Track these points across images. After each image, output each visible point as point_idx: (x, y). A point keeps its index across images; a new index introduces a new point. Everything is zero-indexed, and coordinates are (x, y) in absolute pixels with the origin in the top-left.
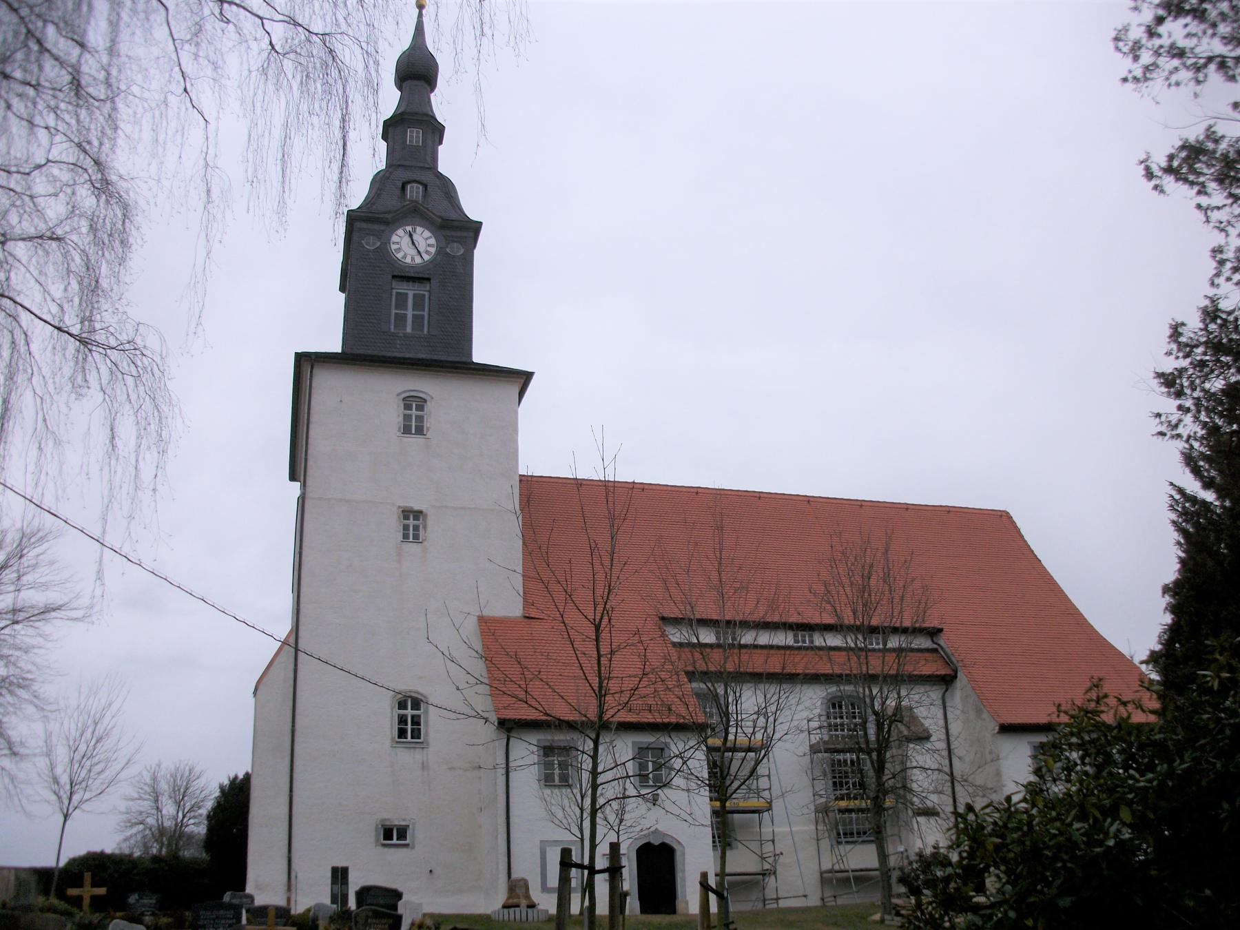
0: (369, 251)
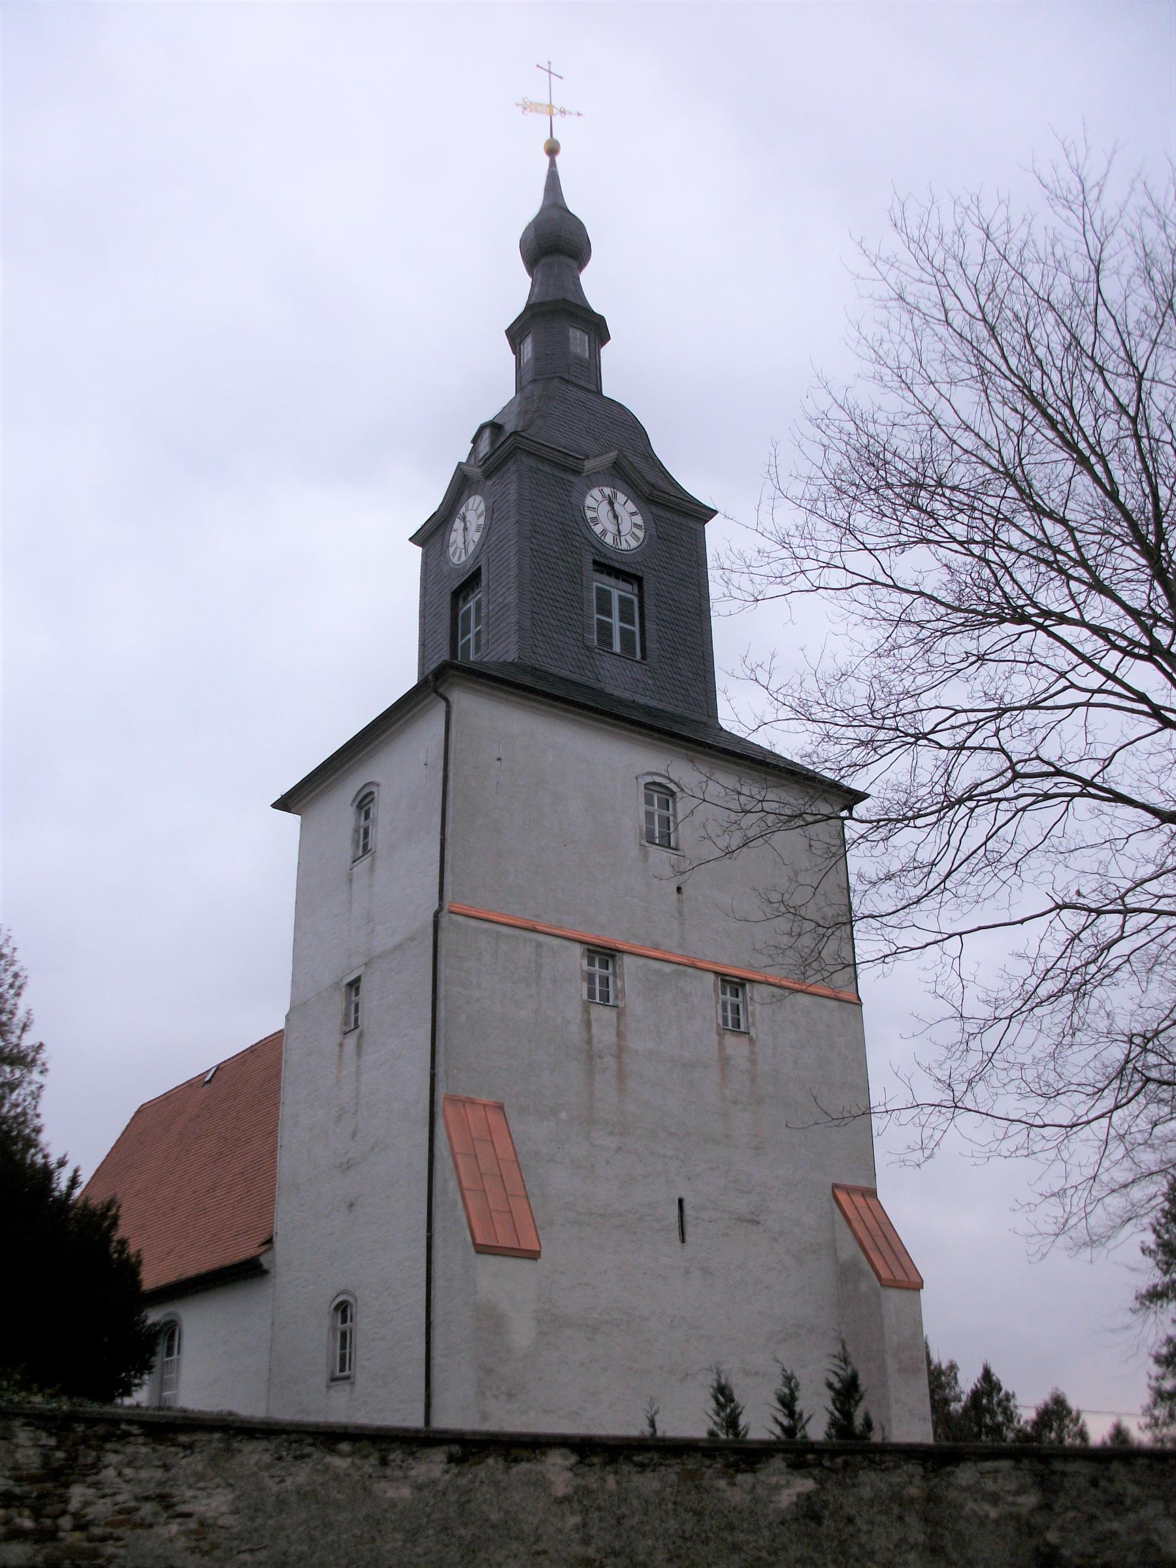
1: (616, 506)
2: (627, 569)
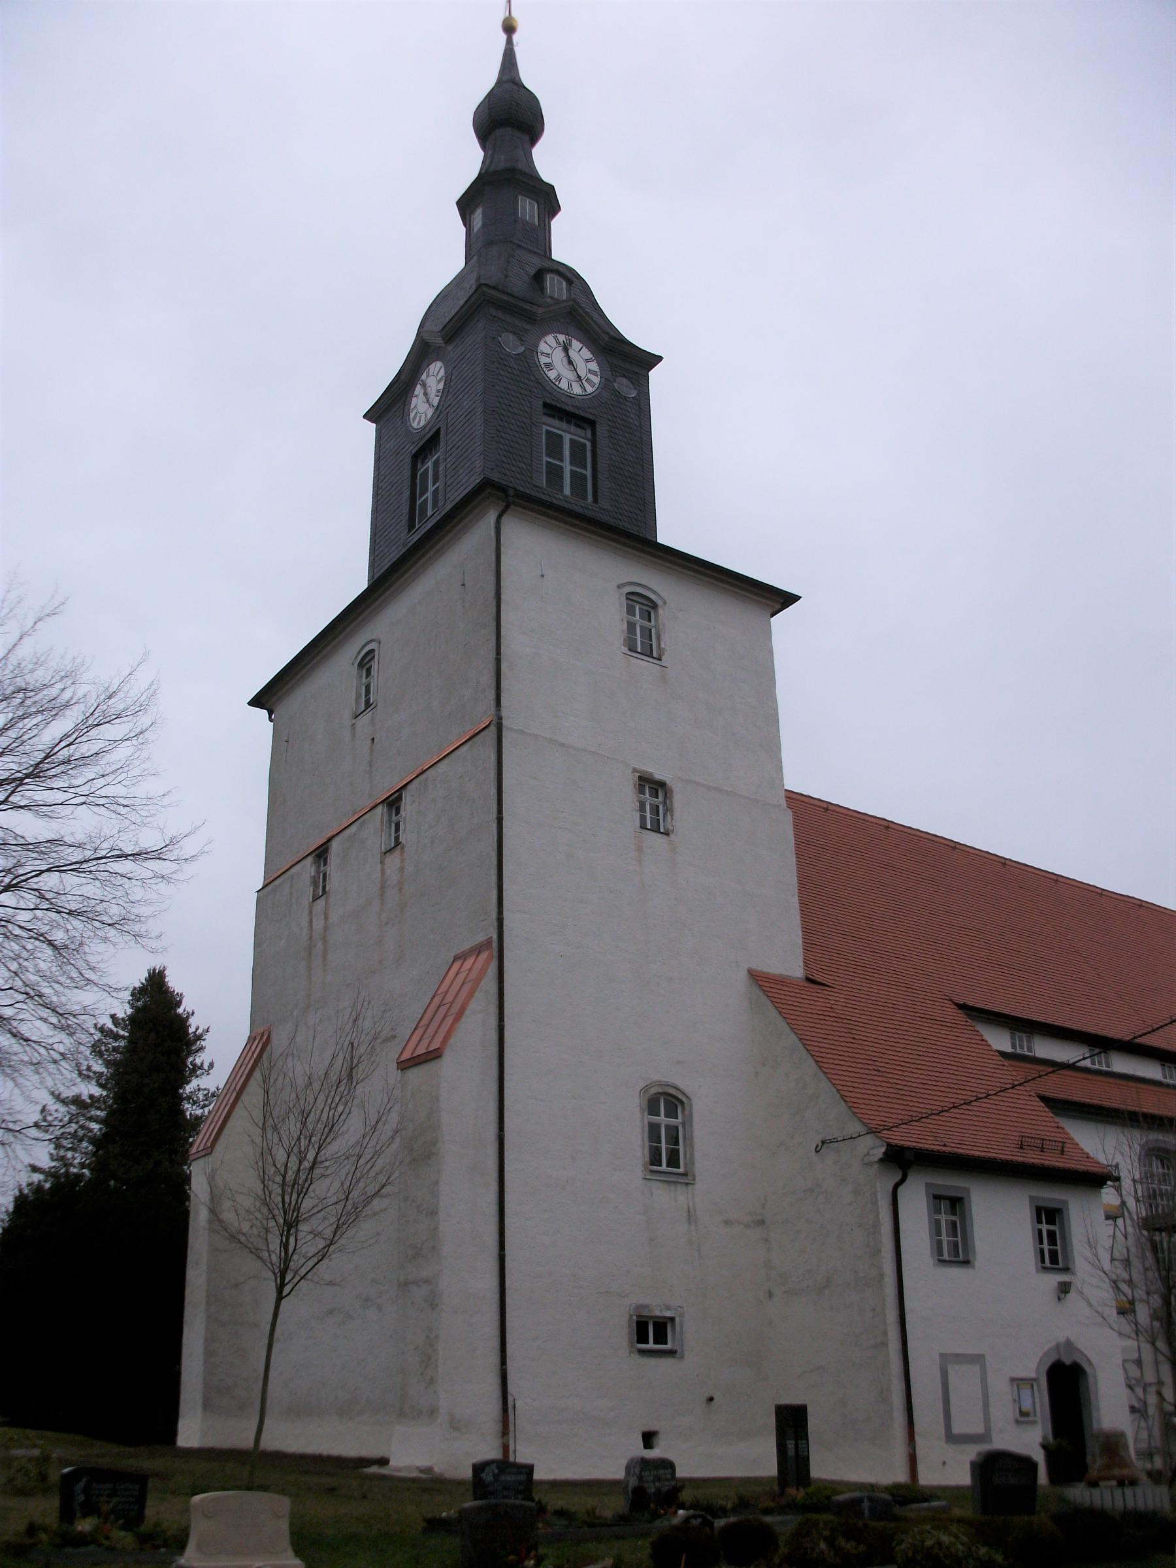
0: (508, 355)
1: (571, 352)
2: (583, 414)
